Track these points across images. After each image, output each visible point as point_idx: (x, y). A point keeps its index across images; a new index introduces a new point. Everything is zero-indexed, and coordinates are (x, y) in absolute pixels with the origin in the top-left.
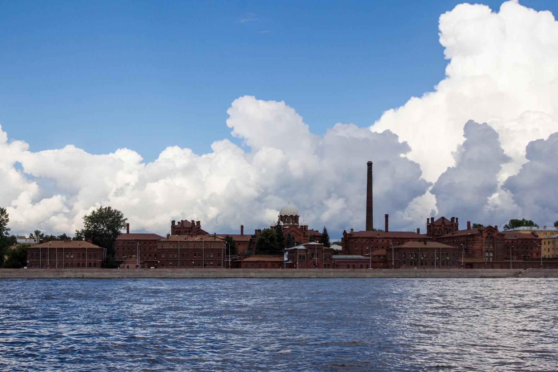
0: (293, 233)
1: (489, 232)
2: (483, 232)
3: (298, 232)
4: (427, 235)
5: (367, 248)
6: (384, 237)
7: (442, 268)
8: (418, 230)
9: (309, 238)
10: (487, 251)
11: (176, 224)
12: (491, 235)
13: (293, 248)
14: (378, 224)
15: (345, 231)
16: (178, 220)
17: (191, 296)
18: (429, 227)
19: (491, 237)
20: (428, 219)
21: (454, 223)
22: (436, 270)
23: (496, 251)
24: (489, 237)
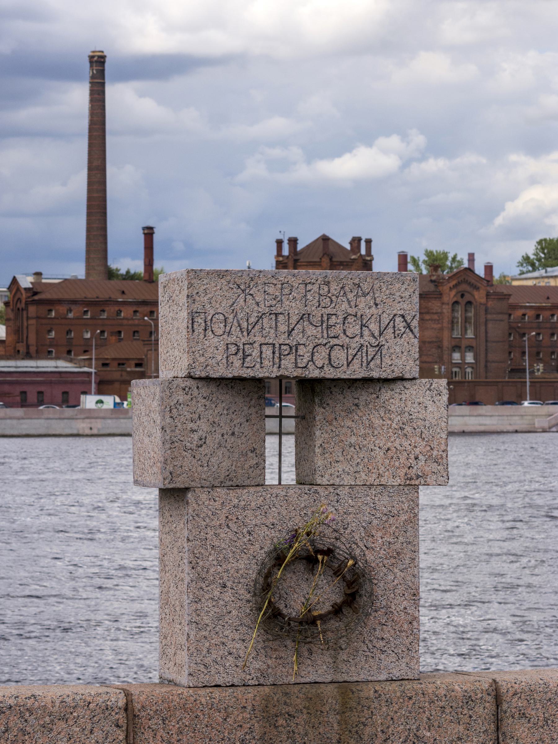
1: (464, 287)
2: (445, 288)
5: (88, 336)
6: (141, 298)
10: (456, 348)
12: (467, 297)
15: (14, 281)
19: (469, 303)
20: (279, 243)
23: (483, 348)
24: (463, 302)
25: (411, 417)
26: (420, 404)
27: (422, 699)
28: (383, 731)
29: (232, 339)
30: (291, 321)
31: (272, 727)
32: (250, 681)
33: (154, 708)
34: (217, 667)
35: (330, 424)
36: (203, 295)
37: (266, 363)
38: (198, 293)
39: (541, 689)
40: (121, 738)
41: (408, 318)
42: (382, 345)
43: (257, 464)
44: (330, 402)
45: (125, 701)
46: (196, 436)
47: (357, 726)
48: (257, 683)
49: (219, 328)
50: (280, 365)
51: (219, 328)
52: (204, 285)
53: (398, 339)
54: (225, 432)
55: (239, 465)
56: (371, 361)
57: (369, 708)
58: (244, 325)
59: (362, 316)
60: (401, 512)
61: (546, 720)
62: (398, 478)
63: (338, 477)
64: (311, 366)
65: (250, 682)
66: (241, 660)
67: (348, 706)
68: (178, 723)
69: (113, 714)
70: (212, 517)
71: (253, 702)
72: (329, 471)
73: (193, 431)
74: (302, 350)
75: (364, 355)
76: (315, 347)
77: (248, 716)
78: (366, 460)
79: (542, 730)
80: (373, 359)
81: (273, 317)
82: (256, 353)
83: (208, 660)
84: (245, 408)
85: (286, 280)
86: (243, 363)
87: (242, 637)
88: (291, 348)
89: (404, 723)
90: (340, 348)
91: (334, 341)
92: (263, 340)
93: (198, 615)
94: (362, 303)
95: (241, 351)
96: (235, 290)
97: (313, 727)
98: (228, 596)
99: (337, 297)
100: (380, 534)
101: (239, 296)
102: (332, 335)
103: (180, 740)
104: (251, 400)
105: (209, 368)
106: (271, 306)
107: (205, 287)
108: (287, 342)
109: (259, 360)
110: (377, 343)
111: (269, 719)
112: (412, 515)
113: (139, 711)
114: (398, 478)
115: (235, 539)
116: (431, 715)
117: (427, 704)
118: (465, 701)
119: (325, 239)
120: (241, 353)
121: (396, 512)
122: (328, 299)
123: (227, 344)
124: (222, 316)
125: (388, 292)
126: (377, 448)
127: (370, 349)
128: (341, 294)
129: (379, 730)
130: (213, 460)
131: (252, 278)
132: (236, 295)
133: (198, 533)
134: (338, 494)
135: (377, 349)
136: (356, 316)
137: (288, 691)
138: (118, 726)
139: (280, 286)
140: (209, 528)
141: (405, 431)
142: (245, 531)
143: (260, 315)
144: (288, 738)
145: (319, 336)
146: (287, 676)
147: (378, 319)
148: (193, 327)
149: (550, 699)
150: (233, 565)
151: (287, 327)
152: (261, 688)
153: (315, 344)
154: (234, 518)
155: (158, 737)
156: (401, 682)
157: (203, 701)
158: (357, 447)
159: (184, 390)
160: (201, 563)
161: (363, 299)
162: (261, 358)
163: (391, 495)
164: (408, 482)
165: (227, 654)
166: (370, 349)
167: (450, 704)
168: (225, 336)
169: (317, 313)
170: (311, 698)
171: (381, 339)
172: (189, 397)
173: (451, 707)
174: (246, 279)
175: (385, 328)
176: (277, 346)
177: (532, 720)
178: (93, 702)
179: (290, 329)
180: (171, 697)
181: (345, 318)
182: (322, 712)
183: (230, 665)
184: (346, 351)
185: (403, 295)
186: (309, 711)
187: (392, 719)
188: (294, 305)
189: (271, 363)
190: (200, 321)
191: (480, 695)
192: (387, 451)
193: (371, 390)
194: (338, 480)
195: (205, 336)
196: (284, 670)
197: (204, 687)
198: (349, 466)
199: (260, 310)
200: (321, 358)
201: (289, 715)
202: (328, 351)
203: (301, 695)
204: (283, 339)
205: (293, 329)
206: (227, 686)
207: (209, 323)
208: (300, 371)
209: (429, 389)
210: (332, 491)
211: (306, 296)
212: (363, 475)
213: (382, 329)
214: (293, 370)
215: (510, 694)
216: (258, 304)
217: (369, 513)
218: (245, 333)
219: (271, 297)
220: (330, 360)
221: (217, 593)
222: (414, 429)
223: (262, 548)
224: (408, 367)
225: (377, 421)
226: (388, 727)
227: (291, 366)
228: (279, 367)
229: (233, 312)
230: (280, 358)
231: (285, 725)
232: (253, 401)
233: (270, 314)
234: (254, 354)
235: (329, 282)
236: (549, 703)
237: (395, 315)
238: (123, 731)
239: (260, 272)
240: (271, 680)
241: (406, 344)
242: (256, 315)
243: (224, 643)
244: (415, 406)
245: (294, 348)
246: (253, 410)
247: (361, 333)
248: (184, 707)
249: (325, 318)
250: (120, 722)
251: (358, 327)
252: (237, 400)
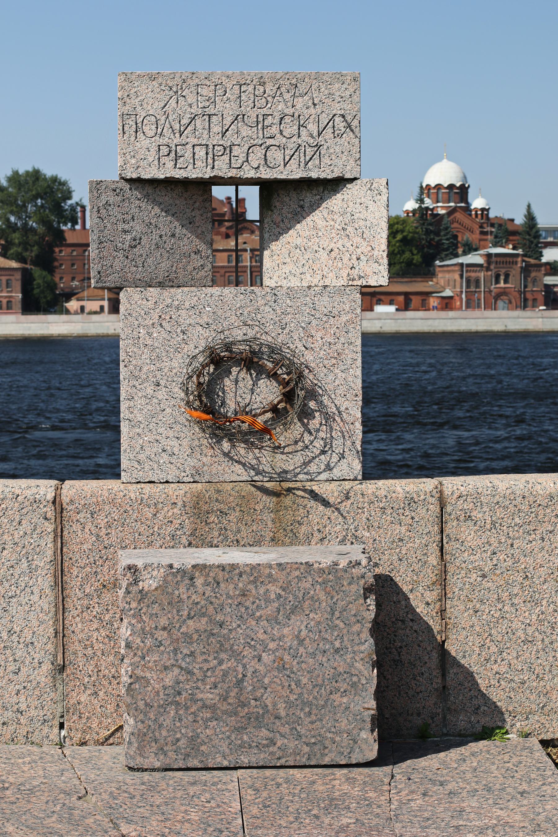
25: (353, 217)
26: (361, 204)
27: (361, 500)
28: (319, 531)
29: (166, 141)
30: (224, 122)
31: (204, 523)
32: (185, 478)
33: (82, 502)
34: (151, 463)
35: (278, 227)
36: (134, 97)
37: (199, 164)
38: (128, 96)
39: (489, 492)
40: (49, 530)
41: (349, 118)
42: (321, 146)
43: (202, 265)
44: (277, 204)
45: (53, 494)
47: (292, 524)
48: (192, 480)
49: (150, 130)
50: (214, 166)
51: (150, 130)
52: (135, 87)
53: (337, 139)
54: (163, 233)
55: (180, 266)
56: (309, 161)
57: (304, 507)
58: (177, 126)
59: (299, 116)
60: (342, 313)
61: (493, 523)
62: (341, 278)
63: (285, 278)
64: (246, 167)
65: (185, 479)
66: (175, 457)
67: (283, 505)
68: (107, 517)
69: (41, 506)
70: (145, 317)
71: (184, 499)
72: (277, 274)
73: (125, 232)
74: (236, 151)
75: (302, 155)
76: (250, 147)
77: (179, 512)
78: (311, 261)
79: (489, 533)
80: (311, 159)
81: (206, 118)
82: (189, 155)
83: (142, 457)
84: (187, 210)
85: (220, 81)
86: (176, 165)
87: (176, 435)
88: (225, 149)
89: (342, 523)
90: (276, 148)
91: (270, 142)
92: (195, 141)
93: (132, 413)
94: (299, 102)
95: (173, 152)
96: (167, 91)
97: (246, 524)
98: (162, 394)
99: (274, 98)
100: (319, 334)
101: (171, 97)
102: (268, 136)
103: (109, 533)
104: (195, 202)
105: (140, 169)
106: (204, 107)
107: (136, 89)
108: (221, 143)
109: (192, 161)
110: (316, 143)
111: (201, 515)
112: (354, 316)
113: (67, 504)
114: (341, 278)
115: (169, 338)
116: (371, 516)
117: (366, 504)
118: (407, 502)
120: (173, 155)
121: (337, 313)
122: (264, 100)
123: (159, 146)
124: (153, 117)
125: (326, 92)
126: (321, 249)
127: (308, 150)
128: (278, 94)
129: (315, 529)
130: (149, 261)
131: (184, 80)
132: (169, 97)
133: (130, 332)
134: (275, 295)
135: (316, 149)
136: (293, 116)
137: (221, 488)
138: (46, 519)
139: (213, 87)
140: (141, 327)
141: (347, 232)
142: (179, 330)
143: (193, 116)
144: (220, 535)
145: (255, 137)
146: (223, 474)
147: (317, 120)
148: (123, 129)
149: (498, 503)
150: (167, 364)
151: (221, 129)
152: (195, 485)
153: (250, 145)
154: (168, 317)
155: (87, 530)
156: (341, 482)
157: (133, 496)
158: (303, 249)
159: (115, 191)
160: (134, 362)
161: (300, 99)
162: (194, 159)
163: (331, 295)
164: (350, 283)
165: (161, 451)
166: (308, 150)
167: (391, 505)
168: (157, 138)
170: (243, 496)
171: (320, 139)
172: (119, 198)
173: (392, 508)
174: (178, 80)
175: (325, 128)
176: (211, 147)
177: (479, 523)
178: (22, 495)
179: (224, 130)
180: (100, 492)
181: (282, 119)
182: (255, 510)
183: (165, 462)
184: (283, 151)
185: (343, 95)
186: (242, 509)
187: (329, 518)
188: (228, 105)
189: (205, 164)
190: (131, 123)
191: (422, 497)
192: (330, 252)
193: (314, 192)
194: (285, 281)
195: (136, 138)
196: (219, 468)
197: (138, 483)
198: (295, 268)
199: (192, 111)
200: (256, 158)
201: (221, 512)
202: (264, 152)
203: (233, 493)
205: (227, 130)
206: (161, 483)
207: (140, 125)
208: (235, 171)
209: (370, 189)
210: (270, 291)
211: (240, 96)
212: (308, 275)
213: (321, 130)
214: (227, 170)
215: (455, 496)
216: (190, 106)
217: (308, 313)
218: (177, 135)
219: (204, 98)
220: (266, 160)
221: (150, 391)
222: (356, 229)
223: (196, 347)
224: (348, 167)
225: (321, 223)
226: (325, 527)
227: (225, 167)
228: (213, 168)
229: (165, 114)
230: (214, 158)
231: (217, 521)
232: (197, 204)
233: (203, 115)
234: (186, 155)
235: (264, 83)
236: (497, 506)
237: (335, 115)
238: (52, 524)
239: (193, 73)
240: (207, 478)
241: (346, 144)
242: (189, 116)
243: (157, 441)
244: (357, 206)
245: (228, 149)
246: (197, 213)
247: (299, 134)
248: (112, 502)
249: (261, 119)
250: (49, 515)
251: (296, 127)
252: (177, 202)
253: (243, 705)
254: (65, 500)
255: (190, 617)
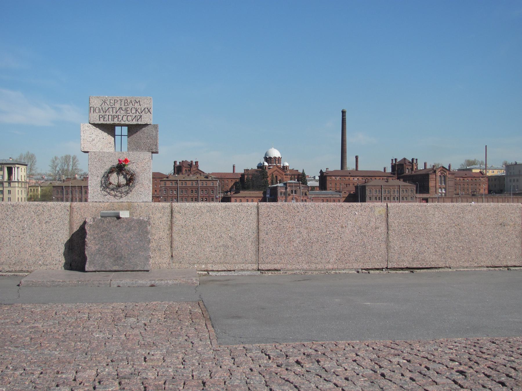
0: (276, 172)
2: (437, 172)
3: (280, 171)
4: (391, 174)
7: (402, 202)
8: (385, 169)
9: (289, 177)
11: (178, 164)
13: (276, 185)
14: (350, 165)
16: (179, 161)
17: (284, 385)
18: (393, 167)
20: (392, 160)
21: (413, 163)
22: (378, 202)
46: (91, 138)
49: (97, 111)
51: (97, 111)
74: (119, 117)
82: (107, 117)
119: (405, 159)
169: (124, 108)
204: (114, 114)
240: (110, 201)
253: (116, 254)
254: (73, 206)
255: (103, 231)
